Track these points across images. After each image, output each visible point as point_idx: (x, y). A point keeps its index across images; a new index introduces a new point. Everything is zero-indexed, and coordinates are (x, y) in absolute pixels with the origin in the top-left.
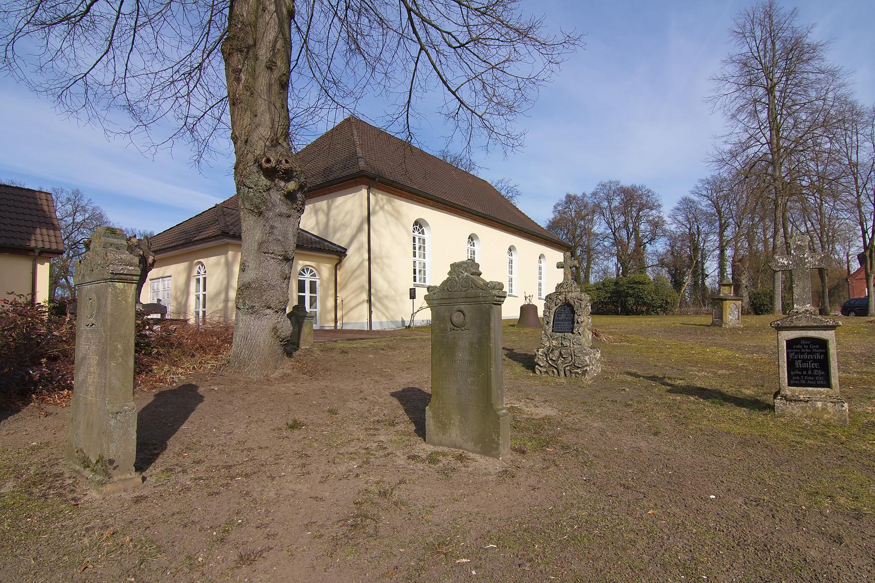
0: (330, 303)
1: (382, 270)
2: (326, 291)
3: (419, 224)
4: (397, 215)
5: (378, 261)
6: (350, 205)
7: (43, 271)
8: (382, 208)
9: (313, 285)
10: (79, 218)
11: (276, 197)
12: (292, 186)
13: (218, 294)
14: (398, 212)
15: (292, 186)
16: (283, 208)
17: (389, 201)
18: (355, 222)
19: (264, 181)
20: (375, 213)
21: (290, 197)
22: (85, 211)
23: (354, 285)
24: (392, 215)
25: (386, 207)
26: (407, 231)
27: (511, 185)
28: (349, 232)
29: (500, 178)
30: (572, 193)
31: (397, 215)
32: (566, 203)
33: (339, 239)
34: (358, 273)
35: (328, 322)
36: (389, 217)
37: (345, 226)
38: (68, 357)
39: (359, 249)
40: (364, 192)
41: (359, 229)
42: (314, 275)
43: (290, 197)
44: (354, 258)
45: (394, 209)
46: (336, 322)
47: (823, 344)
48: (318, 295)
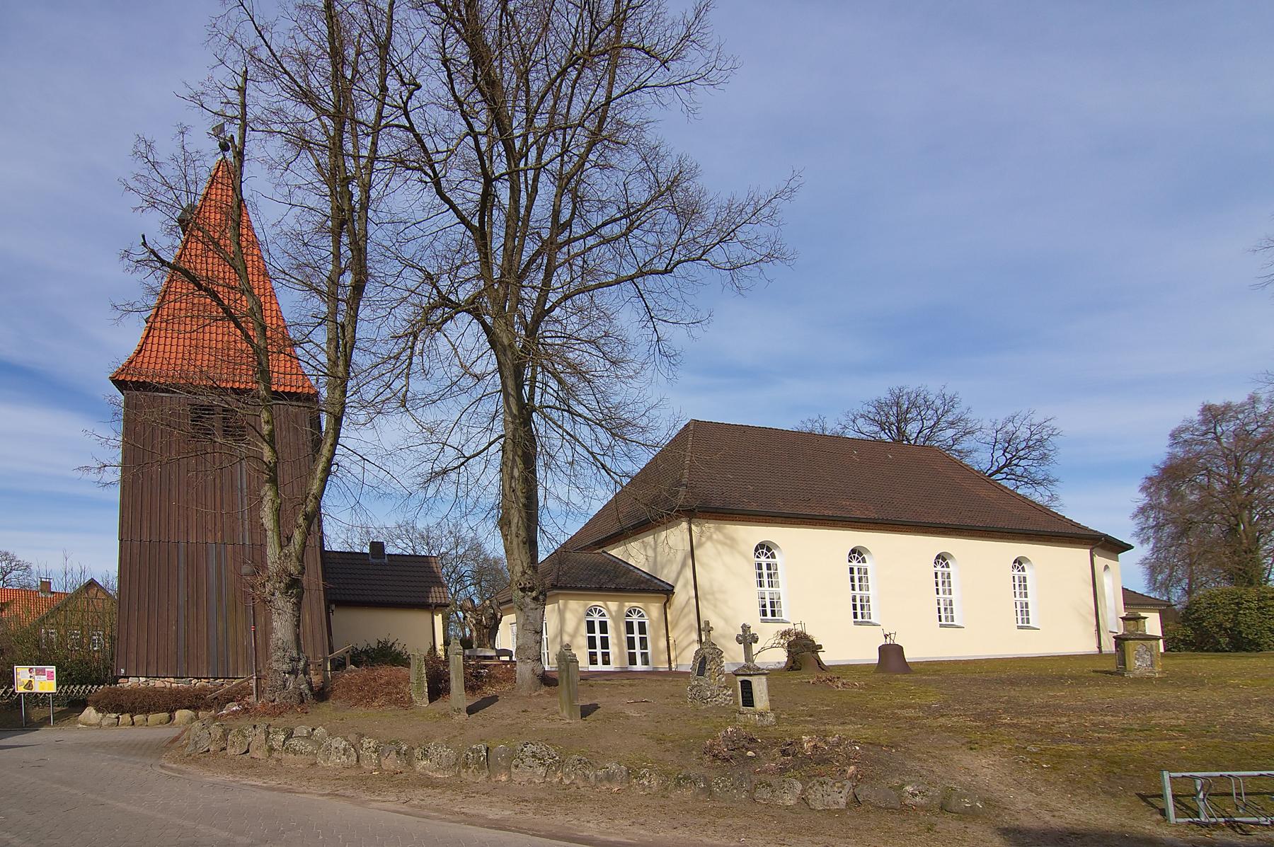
0: (663, 643)
1: (715, 606)
2: (656, 631)
3: (764, 548)
4: (732, 543)
5: (709, 597)
6: (676, 537)
7: (438, 619)
8: (710, 538)
9: (642, 625)
10: (461, 551)
11: (528, 600)
12: (534, 594)
13: (556, 637)
14: (733, 539)
15: (534, 594)
16: (533, 605)
17: (717, 529)
18: (680, 557)
19: (521, 594)
20: (700, 545)
21: (535, 599)
22: (465, 543)
23: (683, 623)
24: (725, 544)
25: (715, 536)
26: (746, 557)
27: (1036, 421)
28: (675, 568)
29: (1009, 414)
30: (1218, 401)
31: (732, 543)
32: (1204, 422)
33: (667, 576)
34: (686, 610)
35: (662, 663)
36: (719, 547)
37: (670, 561)
38: (448, 681)
39: (685, 586)
40: (685, 525)
41: (684, 565)
42: (642, 616)
43: (535, 599)
44: (683, 594)
45: (727, 536)
46: (670, 663)
47: (750, 683)
48: (648, 636)
